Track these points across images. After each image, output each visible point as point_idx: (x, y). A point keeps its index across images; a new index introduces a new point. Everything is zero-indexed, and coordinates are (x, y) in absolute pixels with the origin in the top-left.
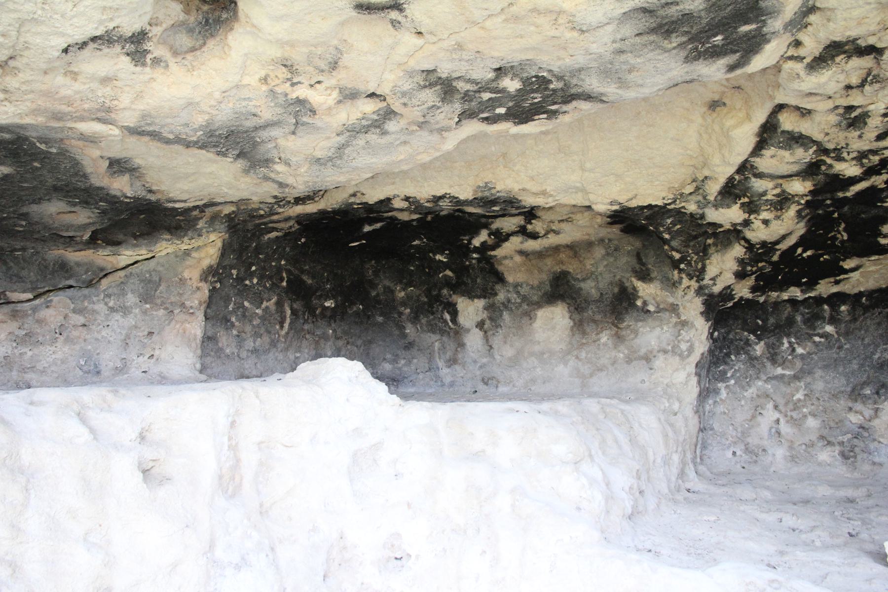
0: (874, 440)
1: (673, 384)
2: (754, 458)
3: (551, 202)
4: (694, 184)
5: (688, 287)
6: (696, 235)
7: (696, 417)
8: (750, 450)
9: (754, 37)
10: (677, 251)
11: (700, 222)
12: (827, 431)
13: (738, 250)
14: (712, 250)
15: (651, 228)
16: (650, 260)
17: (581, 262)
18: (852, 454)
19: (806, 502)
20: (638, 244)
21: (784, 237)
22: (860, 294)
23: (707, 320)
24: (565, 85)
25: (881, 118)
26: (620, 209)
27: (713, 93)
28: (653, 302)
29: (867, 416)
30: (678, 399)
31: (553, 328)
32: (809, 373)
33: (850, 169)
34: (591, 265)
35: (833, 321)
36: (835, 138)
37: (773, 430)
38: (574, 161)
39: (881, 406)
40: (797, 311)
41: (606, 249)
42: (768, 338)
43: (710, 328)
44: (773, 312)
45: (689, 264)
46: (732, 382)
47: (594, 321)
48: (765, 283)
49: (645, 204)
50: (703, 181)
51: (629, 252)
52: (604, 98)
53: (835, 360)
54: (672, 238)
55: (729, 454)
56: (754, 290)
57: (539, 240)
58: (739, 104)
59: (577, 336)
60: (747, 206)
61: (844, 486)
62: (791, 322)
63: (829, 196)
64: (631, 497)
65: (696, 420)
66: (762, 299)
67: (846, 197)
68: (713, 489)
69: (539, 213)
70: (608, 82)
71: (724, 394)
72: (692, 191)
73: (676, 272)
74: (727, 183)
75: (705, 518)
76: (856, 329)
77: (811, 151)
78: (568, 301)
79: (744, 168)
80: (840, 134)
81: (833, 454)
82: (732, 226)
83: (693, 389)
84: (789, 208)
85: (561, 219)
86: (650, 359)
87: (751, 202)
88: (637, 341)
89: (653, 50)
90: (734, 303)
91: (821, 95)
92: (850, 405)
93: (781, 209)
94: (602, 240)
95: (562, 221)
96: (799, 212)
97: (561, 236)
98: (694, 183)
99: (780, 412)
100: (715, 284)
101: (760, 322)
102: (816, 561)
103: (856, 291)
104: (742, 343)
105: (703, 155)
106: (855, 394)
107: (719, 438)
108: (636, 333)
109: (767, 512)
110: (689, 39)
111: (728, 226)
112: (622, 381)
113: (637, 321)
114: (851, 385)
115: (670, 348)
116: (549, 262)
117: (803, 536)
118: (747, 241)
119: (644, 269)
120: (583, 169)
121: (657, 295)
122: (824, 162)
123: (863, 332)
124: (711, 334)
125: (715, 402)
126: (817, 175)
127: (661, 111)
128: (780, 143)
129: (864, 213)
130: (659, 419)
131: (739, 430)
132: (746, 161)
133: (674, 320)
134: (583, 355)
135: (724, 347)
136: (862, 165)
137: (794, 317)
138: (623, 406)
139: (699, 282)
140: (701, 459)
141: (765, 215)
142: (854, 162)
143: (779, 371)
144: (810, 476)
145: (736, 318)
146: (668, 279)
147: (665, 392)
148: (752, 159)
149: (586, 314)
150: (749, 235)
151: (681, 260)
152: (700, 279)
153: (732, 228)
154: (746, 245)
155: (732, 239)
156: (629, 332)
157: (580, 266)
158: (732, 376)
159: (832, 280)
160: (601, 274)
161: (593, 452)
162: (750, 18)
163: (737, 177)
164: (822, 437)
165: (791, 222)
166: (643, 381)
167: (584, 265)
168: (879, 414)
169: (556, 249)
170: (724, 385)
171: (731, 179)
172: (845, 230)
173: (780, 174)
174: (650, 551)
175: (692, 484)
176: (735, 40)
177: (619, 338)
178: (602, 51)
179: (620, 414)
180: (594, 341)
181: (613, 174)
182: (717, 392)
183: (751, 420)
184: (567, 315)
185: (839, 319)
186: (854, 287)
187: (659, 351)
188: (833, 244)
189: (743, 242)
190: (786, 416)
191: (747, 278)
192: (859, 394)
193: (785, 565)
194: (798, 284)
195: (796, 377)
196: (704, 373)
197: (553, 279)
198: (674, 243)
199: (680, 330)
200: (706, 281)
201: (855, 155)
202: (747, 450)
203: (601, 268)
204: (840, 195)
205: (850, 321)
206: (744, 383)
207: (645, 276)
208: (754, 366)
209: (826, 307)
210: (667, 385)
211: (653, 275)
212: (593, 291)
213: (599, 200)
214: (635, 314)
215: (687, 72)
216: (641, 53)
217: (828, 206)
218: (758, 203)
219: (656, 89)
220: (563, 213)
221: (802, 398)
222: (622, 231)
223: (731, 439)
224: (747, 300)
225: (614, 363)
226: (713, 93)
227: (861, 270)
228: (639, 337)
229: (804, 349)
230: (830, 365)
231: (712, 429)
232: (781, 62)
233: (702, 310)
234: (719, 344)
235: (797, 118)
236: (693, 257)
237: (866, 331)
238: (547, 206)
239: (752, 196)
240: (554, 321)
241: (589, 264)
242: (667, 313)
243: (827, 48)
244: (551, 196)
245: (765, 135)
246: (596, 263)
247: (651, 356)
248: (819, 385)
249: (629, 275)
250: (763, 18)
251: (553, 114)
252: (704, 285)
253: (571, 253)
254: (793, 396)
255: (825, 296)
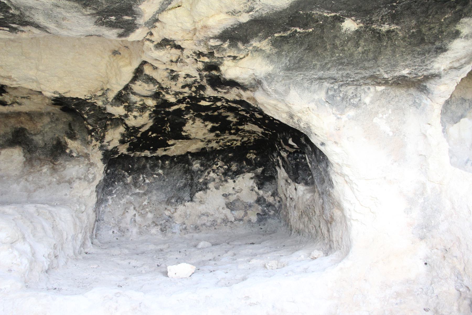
0: (174, 222)
1: (83, 196)
2: (123, 234)
3: (14, 85)
4: (102, 91)
5: (95, 145)
6: (101, 118)
7: (94, 214)
8: (121, 230)
9: (131, 23)
10: (91, 125)
11: (103, 111)
12: (156, 219)
13: (122, 129)
14: (109, 127)
15: (77, 110)
16: (76, 128)
17: (34, 124)
18: (165, 229)
19: (143, 253)
20: (70, 119)
21: (143, 126)
22: (174, 157)
23: (104, 163)
24: (21, 14)
25: (183, 79)
26: (59, 97)
27: (115, 46)
28: (76, 151)
29: (172, 212)
30: (85, 205)
31: (12, 161)
32: (150, 192)
33: (172, 99)
34: (41, 126)
35: (162, 168)
36: (166, 83)
37: (133, 220)
38: (32, 63)
39: (177, 207)
40: (148, 162)
41: (51, 118)
42: (134, 174)
43: (105, 168)
44: (137, 161)
45: (97, 133)
46: (115, 196)
47: (39, 159)
48: (134, 147)
49: (75, 97)
50: (106, 90)
51: (64, 122)
52: (48, 30)
53: (162, 186)
54: (89, 118)
55: (111, 232)
56: (128, 150)
57: (7, 107)
58: (127, 56)
59: (27, 167)
60: (128, 107)
61: (160, 244)
62: (144, 167)
63: (163, 109)
64: (49, 260)
65: (94, 216)
66: (132, 155)
67: (169, 111)
68: (100, 251)
69: (8, 90)
70: (50, 22)
71: (110, 202)
72: (101, 94)
73: (89, 136)
74: (118, 94)
75: (92, 266)
76: (171, 172)
77: (156, 87)
78: (24, 146)
79: (127, 88)
80: (168, 81)
81: (157, 230)
82: (119, 116)
83: (94, 199)
84: (146, 112)
85: (22, 96)
86: (71, 182)
87: (129, 106)
88: (65, 172)
89: (76, 12)
90: (119, 156)
91: (161, 61)
92: (166, 207)
93: (143, 112)
94: (49, 113)
95: (24, 97)
96: (150, 114)
97: (22, 106)
98: (102, 91)
99: (136, 211)
100: (109, 145)
101: (131, 166)
102: (140, 280)
103: (172, 155)
104: (121, 176)
105: (107, 77)
106: (168, 202)
107: (106, 225)
108: (64, 168)
109: (124, 260)
110: (97, 13)
111: (117, 116)
112: (53, 194)
113: (66, 161)
114: (167, 198)
115: (83, 177)
116: (13, 121)
117: (138, 269)
118: (126, 125)
119: (72, 132)
120: (38, 69)
121: (78, 148)
122: (162, 94)
123: (174, 174)
124: (106, 171)
125: (106, 206)
126: (159, 99)
127: (87, 48)
128: (144, 79)
129: (177, 120)
130: (72, 216)
131: (117, 220)
132: (128, 84)
133: (87, 162)
134: (31, 178)
135: (112, 178)
136: (176, 98)
137: (146, 165)
138: (51, 209)
139: (101, 143)
140: (96, 236)
141: (135, 113)
142: (173, 96)
143: (137, 191)
144: (146, 241)
145: (119, 163)
146: (85, 140)
147: (78, 201)
148: (131, 85)
149: (34, 155)
150: (127, 122)
151: (93, 130)
152: (102, 141)
153: (119, 118)
154: (126, 127)
155: (119, 122)
156: (60, 167)
157: (34, 126)
158: (115, 193)
159: (163, 149)
160: (46, 132)
161: (26, 236)
162: (128, 13)
163: (123, 92)
164: (154, 222)
165: (146, 119)
166: (66, 195)
167: (36, 126)
168: (177, 211)
169: (19, 114)
170: (111, 197)
171: (120, 93)
172: (169, 126)
173: (143, 95)
174: (55, 289)
175: (89, 249)
176: (121, 22)
177: (54, 170)
178: (45, 1)
179: (48, 213)
180: (39, 171)
181: (56, 76)
182: (107, 201)
183: (122, 215)
184: (22, 154)
185: (165, 167)
186: (172, 153)
187: (76, 178)
188: (165, 132)
189: (124, 125)
190: (139, 212)
191: (125, 144)
192: (170, 202)
193: (126, 284)
194: (149, 150)
195: (145, 194)
196: (100, 191)
197: (15, 131)
198: (90, 121)
199: (89, 168)
200: (105, 143)
201: (173, 92)
202: (120, 230)
203: (47, 129)
204: (167, 110)
205: (169, 168)
206: (121, 196)
207: (72, 137)
208: (126, 188)
209: (160, 161)
210: (79, 197)
211: (77, 137)
212: (41, 142)
213: (47, 89)
214: (65, 157)
215: (96, 30)
216: (69, 11)
217: (163, 114)
218: (132, 107)
219: (79, 34)
220: (25, 94)
221: (146, 204)
222: (61, 109)
223: (112, 225)
224: (125, 155)
225: (50, 184)
226: (115, 46)
227: (175, 146)
228: (66, 170)
229: (149, 180)
230: (160, 188)
231: (103, 220)
232: (144, 40)
233: (102, 158)
234: (110, 176)
235: (152, 70)
236: (99, 130)
237: (175, 173)
238: (12, 86)
239: (130, 103)
240: (13, 157)
241: (39, 126)
242: (83, 158)
243: (163, 40)
244: (15, 81)
245: (137, 74)
246: (44, 126)
247: (72, 181)
248: (154, 198)
249: (64, 135)
250: (135, 16)
251: (13, 30)
252: (104, 145)
253: (28, 118)
254: (143, 203)
255: (160, 156)
